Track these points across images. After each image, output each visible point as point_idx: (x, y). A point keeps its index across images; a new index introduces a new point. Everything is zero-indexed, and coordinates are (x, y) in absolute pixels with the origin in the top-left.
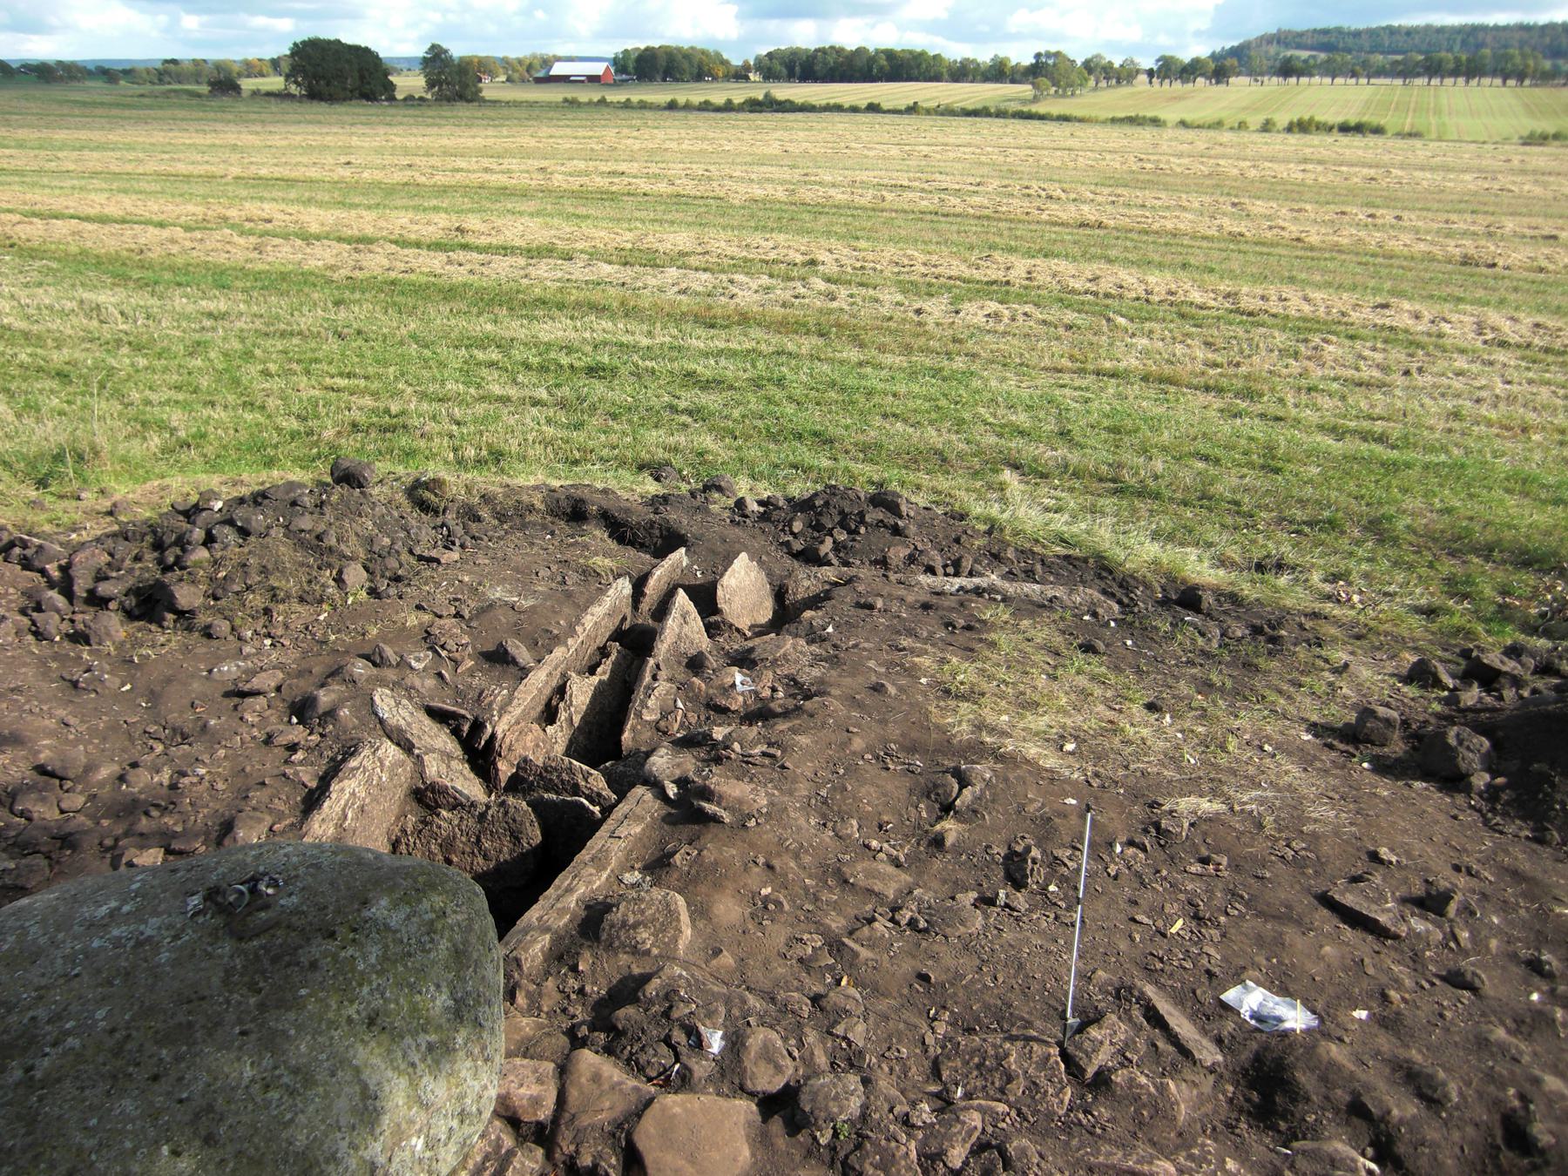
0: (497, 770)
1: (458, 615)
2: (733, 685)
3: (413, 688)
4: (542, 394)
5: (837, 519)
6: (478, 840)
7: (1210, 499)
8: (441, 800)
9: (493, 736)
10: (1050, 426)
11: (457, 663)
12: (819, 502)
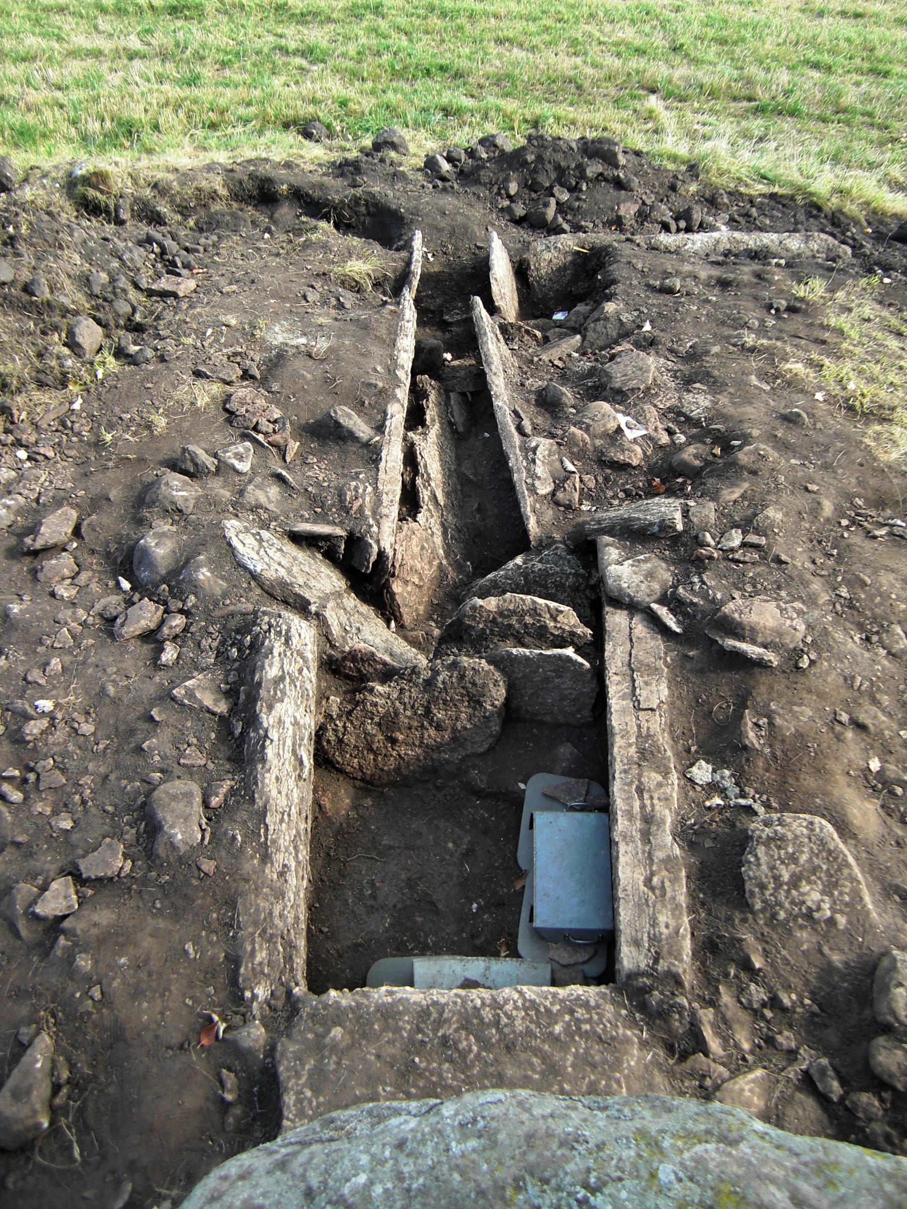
0: (393, 595)
1: (246, 375)
2: (619, 430)
3: (259, 506)
4: (134, 43)
5: (553, 176)
6: (428, 711)
7: (845, 111)
8: (366, 669)
9: (381, 554)
10: (659, 41)
11: (282, 451)
12: (530, 158)
